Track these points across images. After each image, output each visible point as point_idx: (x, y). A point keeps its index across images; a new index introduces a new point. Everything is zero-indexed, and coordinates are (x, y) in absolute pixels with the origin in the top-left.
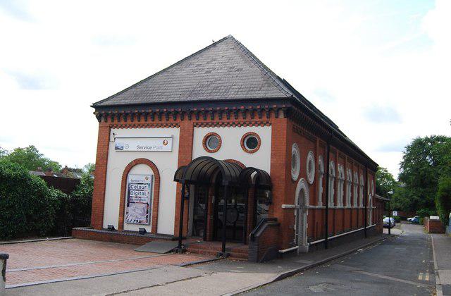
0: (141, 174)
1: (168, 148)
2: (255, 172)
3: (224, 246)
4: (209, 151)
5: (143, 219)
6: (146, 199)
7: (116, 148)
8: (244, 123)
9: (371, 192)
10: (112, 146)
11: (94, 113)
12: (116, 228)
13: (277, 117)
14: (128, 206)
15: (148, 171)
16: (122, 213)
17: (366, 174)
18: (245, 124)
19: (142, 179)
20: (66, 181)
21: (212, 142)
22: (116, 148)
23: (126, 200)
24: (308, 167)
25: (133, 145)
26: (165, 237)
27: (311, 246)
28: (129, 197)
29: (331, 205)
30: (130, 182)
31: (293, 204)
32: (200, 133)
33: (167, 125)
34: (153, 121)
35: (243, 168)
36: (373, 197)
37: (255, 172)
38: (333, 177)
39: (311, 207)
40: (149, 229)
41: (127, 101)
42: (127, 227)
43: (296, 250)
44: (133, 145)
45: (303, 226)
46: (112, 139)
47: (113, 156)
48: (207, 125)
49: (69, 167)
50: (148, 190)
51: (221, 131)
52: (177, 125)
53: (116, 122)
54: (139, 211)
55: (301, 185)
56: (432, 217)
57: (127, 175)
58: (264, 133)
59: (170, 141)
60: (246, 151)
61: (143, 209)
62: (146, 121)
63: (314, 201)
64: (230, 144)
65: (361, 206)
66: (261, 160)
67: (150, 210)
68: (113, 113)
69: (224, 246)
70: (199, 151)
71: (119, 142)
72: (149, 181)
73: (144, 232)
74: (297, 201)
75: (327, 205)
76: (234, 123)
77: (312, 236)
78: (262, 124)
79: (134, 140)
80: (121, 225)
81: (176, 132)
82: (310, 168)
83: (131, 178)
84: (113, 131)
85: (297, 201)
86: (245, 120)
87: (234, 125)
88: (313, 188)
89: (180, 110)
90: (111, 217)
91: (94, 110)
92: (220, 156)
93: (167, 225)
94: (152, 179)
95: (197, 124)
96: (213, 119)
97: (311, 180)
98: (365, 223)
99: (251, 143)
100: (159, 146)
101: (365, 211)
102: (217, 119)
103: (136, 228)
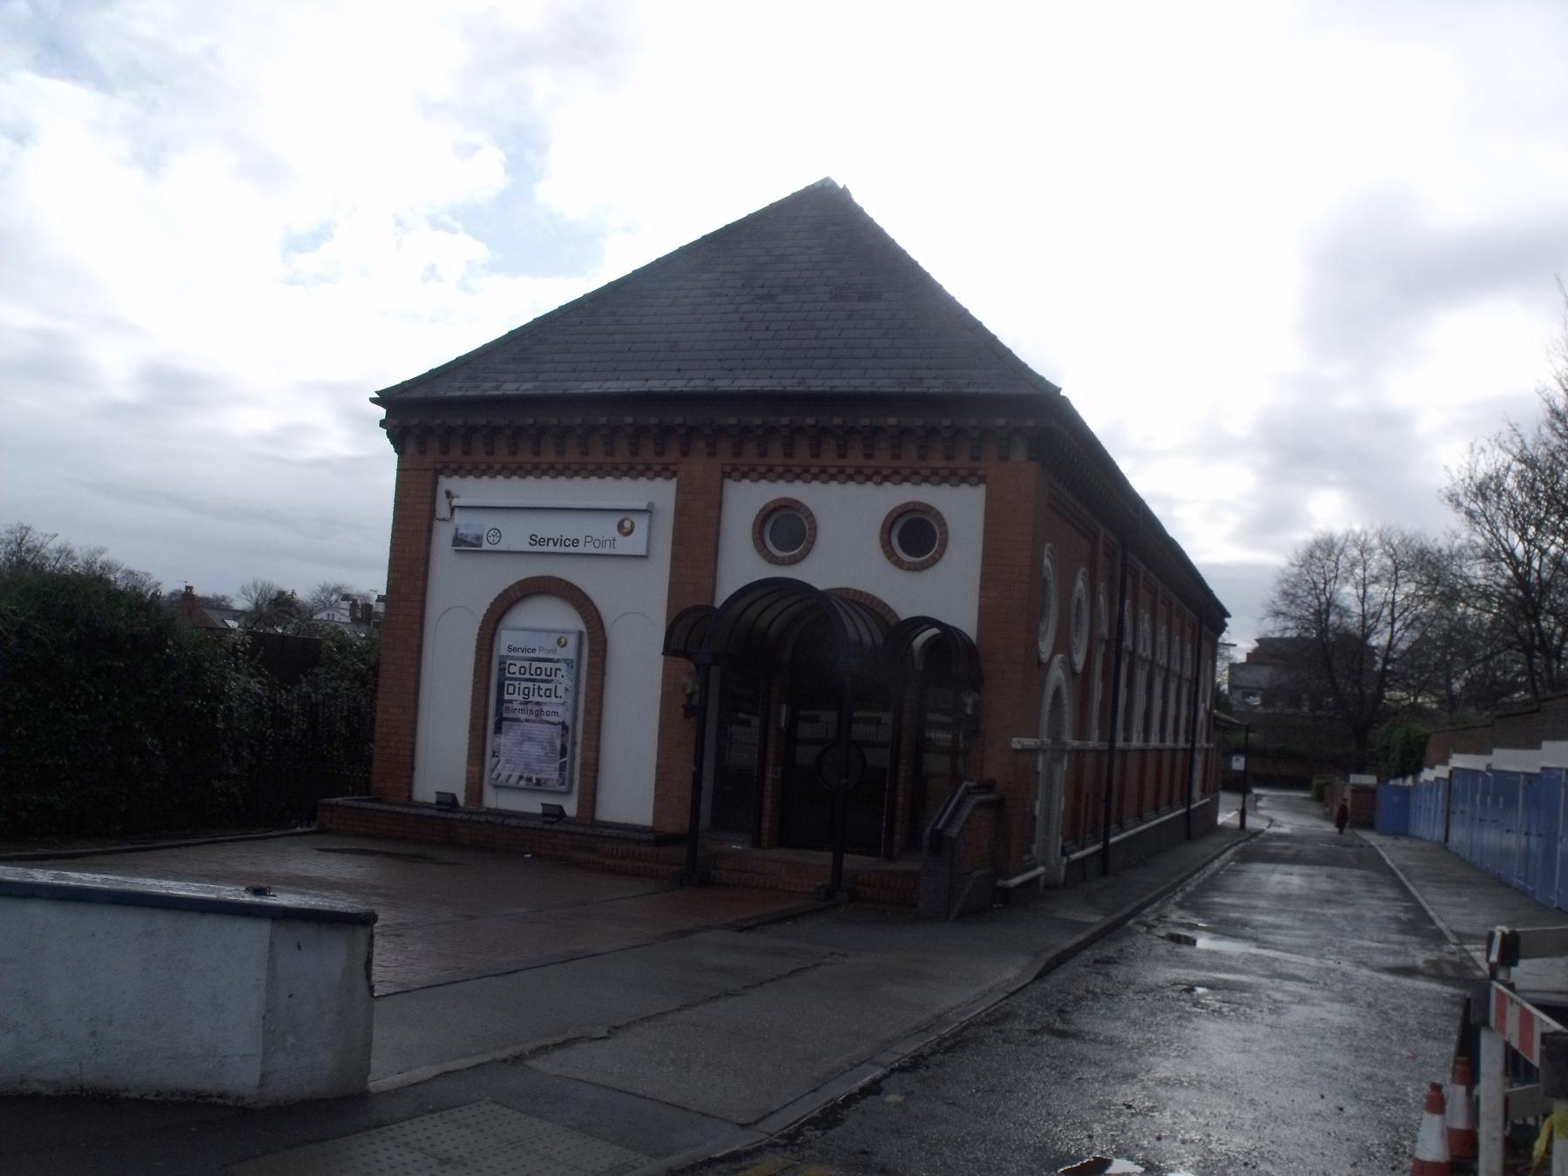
0: (542, 627)
1: (635, 544)
2: (934, 631)
3: (838, 861)
4: (773, 560)
5: (551, 773)
6: (560, 710)
7: (458, 541)
8: (842, 471)
9: (1204, 701)
10: (443, 536)
11: (383, 424)
12: (461, 800)
13: (1004, 458)
14: (498, 729)
15: (566, 619)
16: (478, 752)
17: (1199, 648)
18: (895, 476)
19: (544, 646)
20: (283, 638)
21: (787, 529)
22: (458, 541)
23: (490, 710)
24: (1073, 619)
25: (515, 533)
26: (626, 834)
27: (1070, 865)
28: (500, 701)
29: (1120, 744)
30: (504, 651)
31: (1036, 736)
32: (745, 501)
33: (490, 467)
34: (586, 453)
35: (892, 622)
36: (1209, 714)
37: (934, 631)
38: (1144, 661)
39: (1076, 744)
40: (571, 808)
41: (671, 384)
42: (493, 800)
43: (1036, 879)
44: (515, 533)
45: (1051, 805)
46: (442, 509)
47: (446, 567)
48: (770, 474)
49: (199, 591)
50: (563, 681)
51: (815, 496)
52: (665, 472)
53: (456, 453)
54: (533, 750)
55: (1057, 674)
56: (1356, 779)
57: (495, 629)
58: (962, 509)
59: (641, 523)
60: (898, 563)
61: (551, 743)
62: (561, 453)
63: (1081, 732)
64: (845, 538)
65: (1182, 744)
66: (948, 594)
67: (574, 744)
68: (441, 423)
69: (838, 861)
70: (741, 565)
71: (467, 524)
72: (569, 652)
73: (559, 813)
74: (1044, 726)
75: (1112, 740)
76: (859, 471)
77: (1075, 837)
78: (954, 477)
79: (514, 514)
80: (475, 788)
81: (661, 493)
82: (1078, 622)
83: (506, 639)
84: (446, 483)
85: (1044, 726)
86: (537, 460)
87: (860, 475)
88: (1082, 680)
89: (679, 420)
90: (440, 762)
91: (381, 412)
92: (821, 570)
93: (630, 792)
94: (580, 644)
95: (735, 468)
96: (788, 455)
97: (1079, 660)
98: (1187, 798)
99: (915, 537)
100: (610, 538)
101: (1190, 753)
102: (802, 455)
103: (532, 804)
